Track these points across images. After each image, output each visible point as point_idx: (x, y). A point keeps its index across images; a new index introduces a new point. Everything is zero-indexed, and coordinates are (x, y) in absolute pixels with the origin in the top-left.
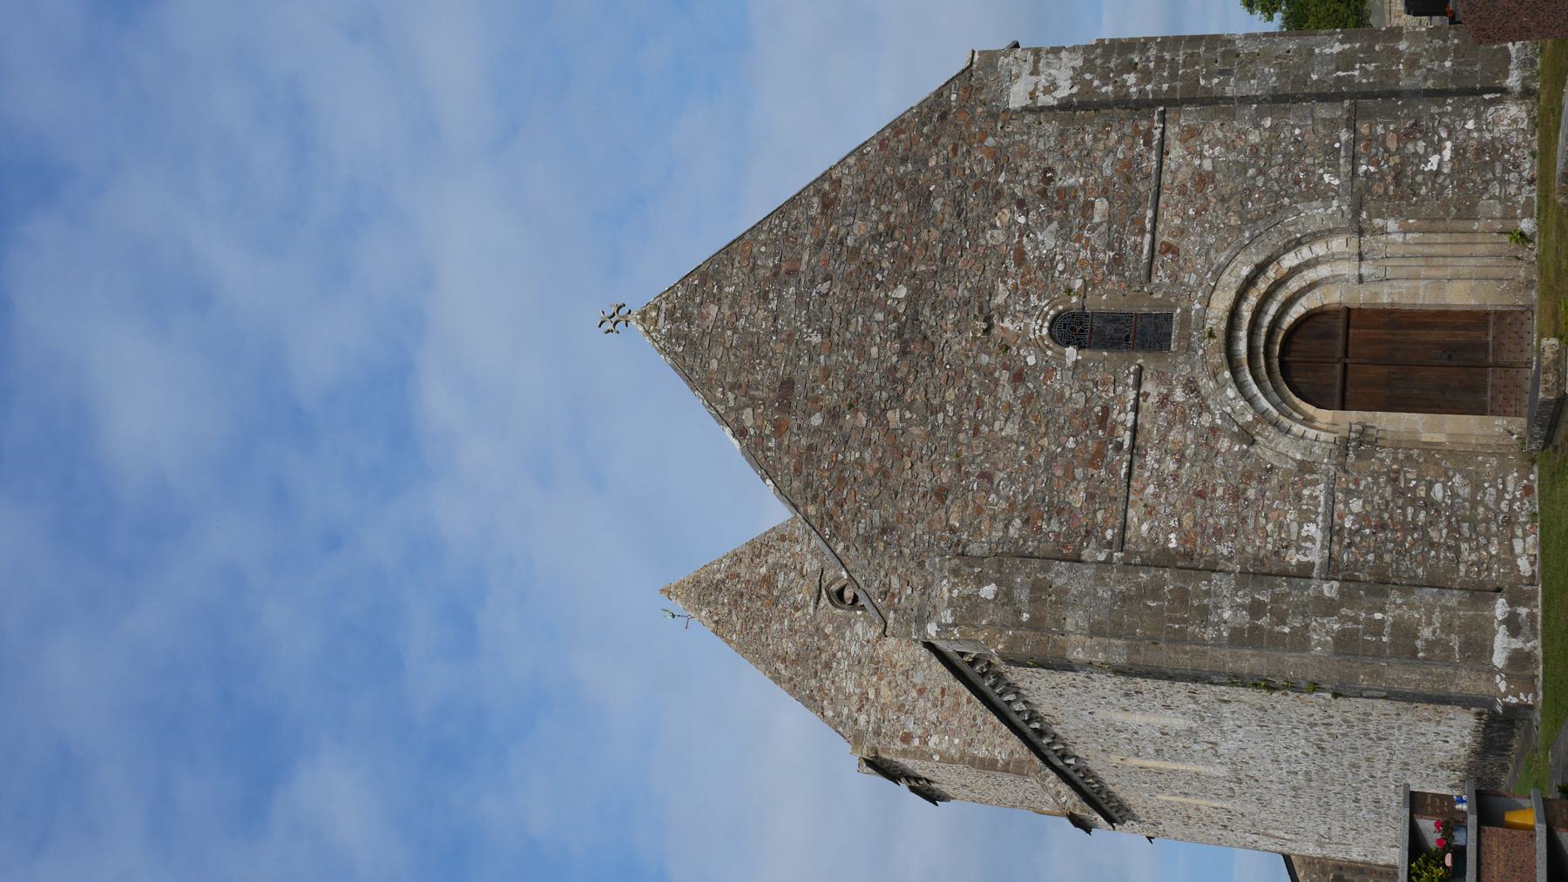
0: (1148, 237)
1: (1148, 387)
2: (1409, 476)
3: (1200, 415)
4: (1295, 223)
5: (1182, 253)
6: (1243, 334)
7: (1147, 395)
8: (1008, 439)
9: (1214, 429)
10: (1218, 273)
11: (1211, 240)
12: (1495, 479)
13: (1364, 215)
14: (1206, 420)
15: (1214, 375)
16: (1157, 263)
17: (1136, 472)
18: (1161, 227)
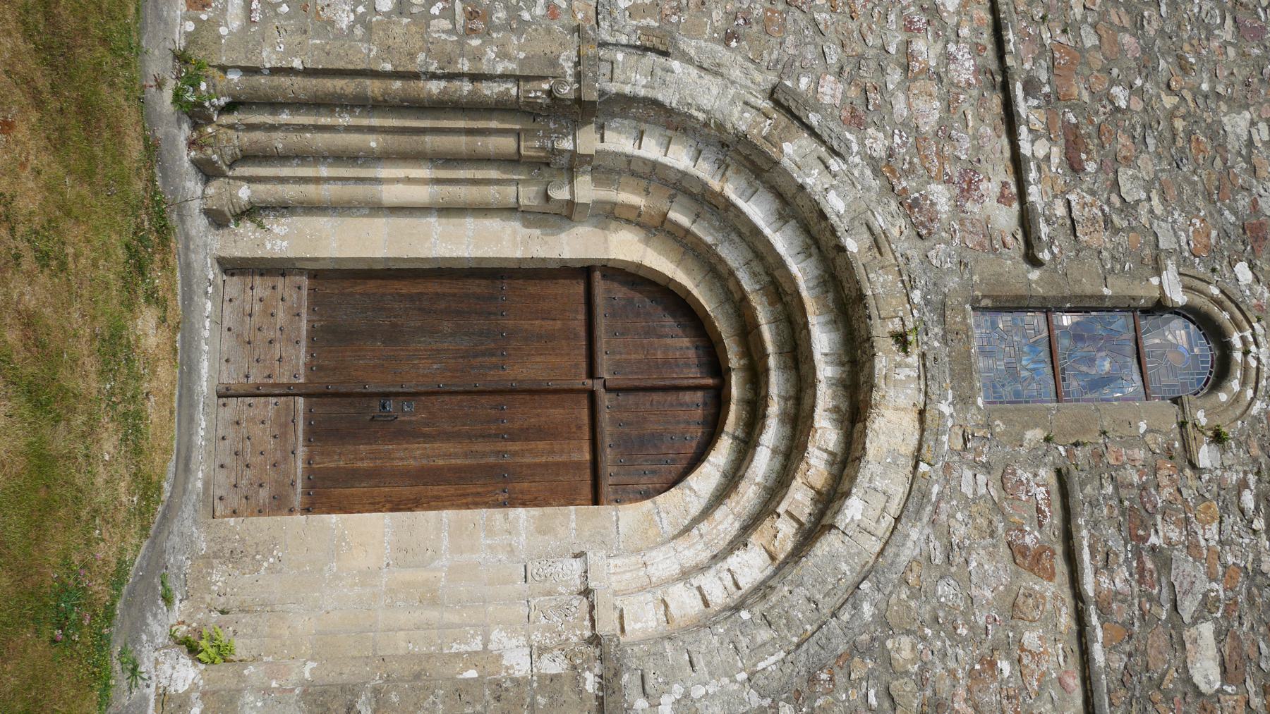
0: (1089, 587)
1: (1006, 218)
2: (446, 24)
3: (891, 153)
4: (758, 650)
5: (1003, 550)
6: (825, 371)
7: (1003, 198)
8: (1238, 105)
9: (856, 121)
10: (915, 496)
11: (946, 590)
12: (265, 20)
13: (590, 683)
14: (877, 143)
15: (877, 242)
16: (1054, 520)
17: (986, 38)
18: (1066, 620)
